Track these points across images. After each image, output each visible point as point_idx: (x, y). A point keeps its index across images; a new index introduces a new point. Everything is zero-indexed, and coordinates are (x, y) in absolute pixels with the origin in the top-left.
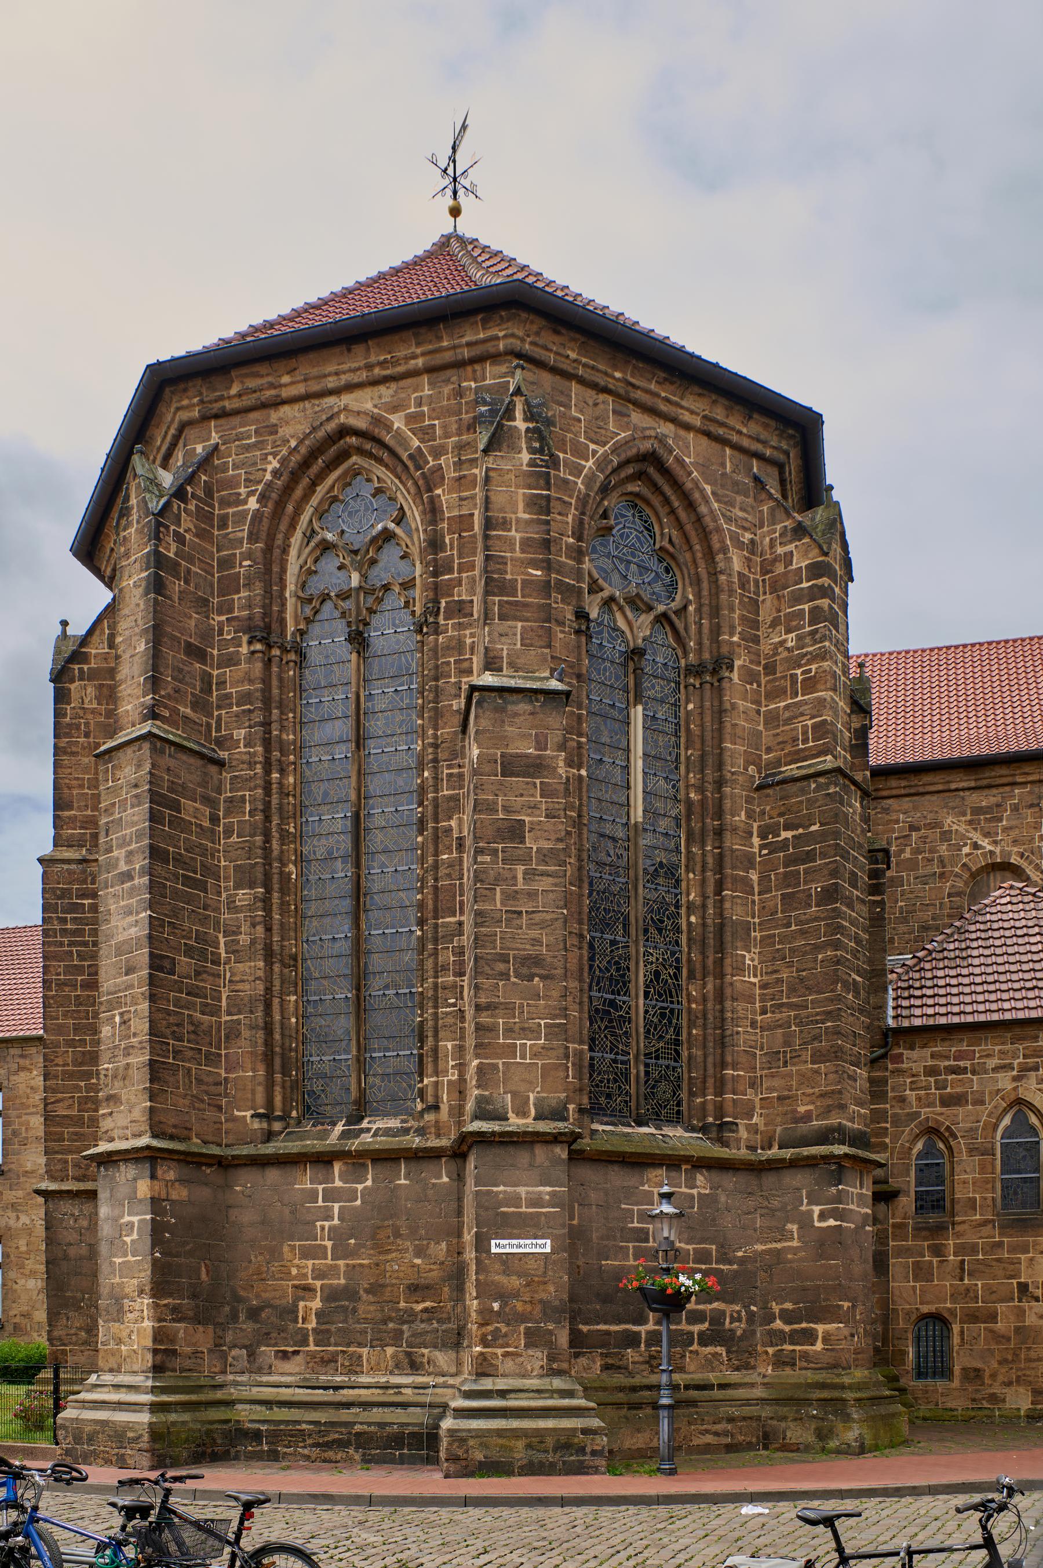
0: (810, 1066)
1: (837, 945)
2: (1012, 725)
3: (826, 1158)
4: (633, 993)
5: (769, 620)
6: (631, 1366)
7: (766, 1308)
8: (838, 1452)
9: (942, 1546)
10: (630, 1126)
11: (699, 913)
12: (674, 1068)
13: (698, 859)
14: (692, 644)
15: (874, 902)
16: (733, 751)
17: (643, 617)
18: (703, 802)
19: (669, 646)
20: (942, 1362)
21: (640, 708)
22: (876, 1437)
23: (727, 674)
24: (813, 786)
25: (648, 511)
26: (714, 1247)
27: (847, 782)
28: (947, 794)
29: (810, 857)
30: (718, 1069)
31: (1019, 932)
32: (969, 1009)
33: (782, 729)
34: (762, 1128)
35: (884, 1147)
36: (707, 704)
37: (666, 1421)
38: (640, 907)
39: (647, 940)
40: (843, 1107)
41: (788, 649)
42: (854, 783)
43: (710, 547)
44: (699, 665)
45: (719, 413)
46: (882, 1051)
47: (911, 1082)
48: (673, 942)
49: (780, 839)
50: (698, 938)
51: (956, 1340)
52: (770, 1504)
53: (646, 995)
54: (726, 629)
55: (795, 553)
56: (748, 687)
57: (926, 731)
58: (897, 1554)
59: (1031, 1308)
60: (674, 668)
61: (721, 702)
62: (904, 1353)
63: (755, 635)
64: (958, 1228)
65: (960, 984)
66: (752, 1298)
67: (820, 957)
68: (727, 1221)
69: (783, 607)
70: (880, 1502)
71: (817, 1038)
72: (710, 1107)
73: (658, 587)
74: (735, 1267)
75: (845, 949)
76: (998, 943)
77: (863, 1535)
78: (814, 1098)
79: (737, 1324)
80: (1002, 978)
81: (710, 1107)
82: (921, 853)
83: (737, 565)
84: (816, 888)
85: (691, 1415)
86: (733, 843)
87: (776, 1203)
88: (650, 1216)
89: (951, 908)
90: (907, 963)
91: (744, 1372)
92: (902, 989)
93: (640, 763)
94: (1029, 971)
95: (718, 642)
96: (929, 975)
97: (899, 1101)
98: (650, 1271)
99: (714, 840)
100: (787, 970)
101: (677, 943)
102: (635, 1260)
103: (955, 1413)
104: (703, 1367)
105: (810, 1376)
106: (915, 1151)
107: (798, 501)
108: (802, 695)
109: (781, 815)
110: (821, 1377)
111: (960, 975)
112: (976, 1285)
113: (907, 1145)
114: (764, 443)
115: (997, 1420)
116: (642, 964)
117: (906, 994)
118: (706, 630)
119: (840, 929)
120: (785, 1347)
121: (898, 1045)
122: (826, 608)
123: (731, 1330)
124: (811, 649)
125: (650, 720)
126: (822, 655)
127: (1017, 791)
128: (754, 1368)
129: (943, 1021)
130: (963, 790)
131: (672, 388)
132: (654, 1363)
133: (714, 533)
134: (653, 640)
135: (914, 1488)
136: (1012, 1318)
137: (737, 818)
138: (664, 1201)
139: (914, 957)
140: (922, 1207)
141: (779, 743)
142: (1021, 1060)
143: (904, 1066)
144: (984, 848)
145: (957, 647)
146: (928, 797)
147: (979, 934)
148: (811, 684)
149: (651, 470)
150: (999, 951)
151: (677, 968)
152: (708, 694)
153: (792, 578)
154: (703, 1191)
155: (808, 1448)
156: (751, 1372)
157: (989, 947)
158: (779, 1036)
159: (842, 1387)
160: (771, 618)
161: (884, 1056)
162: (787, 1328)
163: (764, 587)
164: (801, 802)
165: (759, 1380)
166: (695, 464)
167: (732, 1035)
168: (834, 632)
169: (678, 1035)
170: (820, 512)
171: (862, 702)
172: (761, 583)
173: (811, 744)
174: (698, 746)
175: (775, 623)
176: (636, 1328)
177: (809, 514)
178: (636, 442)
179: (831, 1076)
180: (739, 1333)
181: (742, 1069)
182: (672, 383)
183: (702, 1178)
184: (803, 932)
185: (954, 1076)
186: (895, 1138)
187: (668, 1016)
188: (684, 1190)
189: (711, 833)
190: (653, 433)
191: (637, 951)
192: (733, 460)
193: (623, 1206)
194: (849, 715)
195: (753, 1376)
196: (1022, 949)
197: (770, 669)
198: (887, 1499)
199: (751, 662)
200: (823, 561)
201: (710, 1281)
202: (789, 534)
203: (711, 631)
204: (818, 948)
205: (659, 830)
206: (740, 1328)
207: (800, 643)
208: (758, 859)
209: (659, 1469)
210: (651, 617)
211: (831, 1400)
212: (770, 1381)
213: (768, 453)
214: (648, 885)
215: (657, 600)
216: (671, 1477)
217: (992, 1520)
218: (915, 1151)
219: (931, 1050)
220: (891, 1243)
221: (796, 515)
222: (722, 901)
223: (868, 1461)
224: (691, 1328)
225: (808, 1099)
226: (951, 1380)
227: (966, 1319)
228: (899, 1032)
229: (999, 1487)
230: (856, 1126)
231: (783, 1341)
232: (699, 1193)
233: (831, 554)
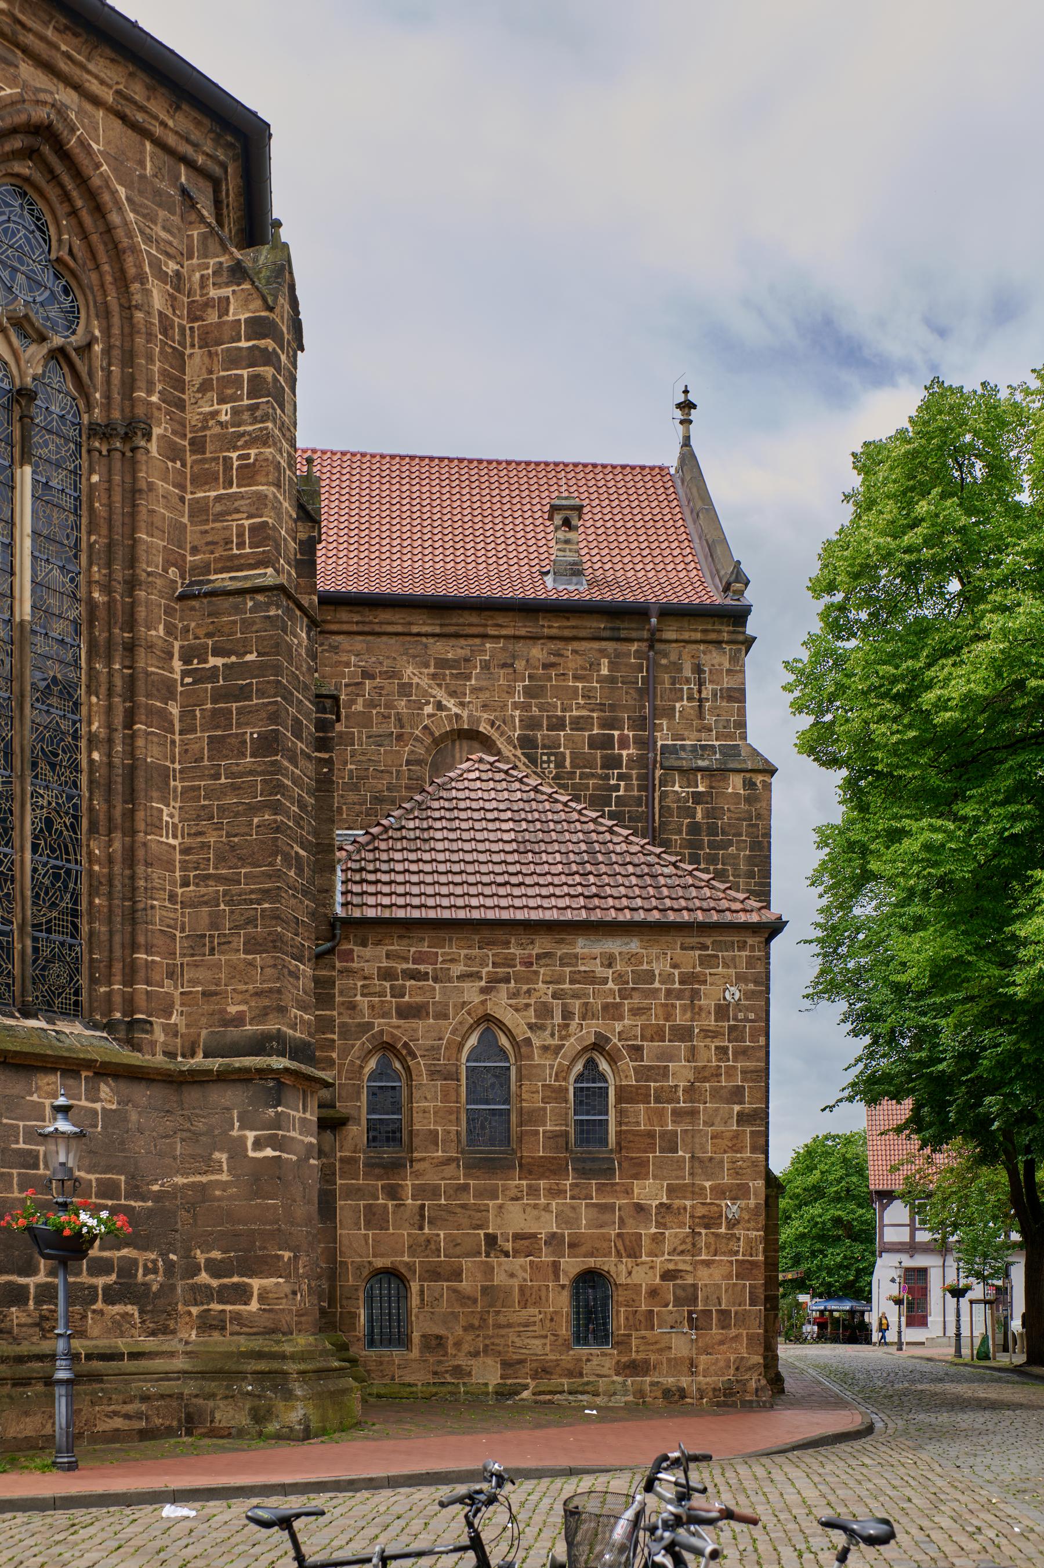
0: (243, 956)
1: (276, 808)
2: (484, 565)
3: (263, 1073)
4: (17, 844)
5: (197, 382)
6: (16, 1330)
7: (188, 1257)
8: (278, 1437)
9: (407, 1550)
10: (14, 1017)
11: (104, 748)
12: (71, 946)
13: (103, 678)
14: (98, 395)
15: (320, 759)
16: (150, 546)
17: (33, 348)
18: (110, 605)
19: (67, 394)
20: (399, 1326)
21: (28, 470)
22: (323, 1419)
23: (143, 443)
24: (250, 604)
25: (41, 205)
26: (123, 1178)
27: (292, 605)
28: (408, 638)
29: (243, 693)
30: (127, 952)
31: (490, 816)
32: (431, 902)
33: (211, 525)
34: (183, 1029)
35: (330, 1063)
36: (117, 478)
37: (63, 1400)
38: (27, 733)
39: (36, 777)
40: (282, 1010)
41: (220, 423)
42: (300, 607)
43: (123, 271)
44: (107, 426)
45: (138, 91)
46: (329, 945)
47: (362, 986)
48: (70, 783)
49: (207, 666)
50: (102, 781)
51: (415, 1301)
52: (198, 1505)
53: (35, 848)
54: (141, 384)
55: (232, 300)
56: (170, 464)
57: (384, 557)
58: (369, 1560)
59: (500, 1264)
60: (74, 424)
61: (135, 479)
62: (354, 1316)
63: (180, 398)
64: (417, 1166)
65: (421, 871)
66: (170, 1244)
67: (256, 820)
68: (140, 1146)
69: (215, 368)
70: (331, 1498)
71: (251, 922)
72: (117, 999)
73: (53, 311)
74: (150, 1204)
75: (287, 813)
76: (465, 825)
77: (313, 1540)
78: (247, 996)
79: (152, 1276)
80: (470, 868)
81: (117, 999)
82: (375, 707)
83: (158, 301)
84: (252, 734)
85: (94, 1393)
86: (148, 664)
87: (200, 1126)
88: (40, 1135)
89: (409, 779)
90: (359, 839)
91: (162, 1338)
92: (353, 870)
93: (28, 543)
94: (500, 863)
95: (131, 399)
96: (384, 856)
97: (348, 1008)
98: (42, 1206)
99: (123, 658)
100: (215, 833)
101: (75, 784)
102: (21, 1191)
103: (414, 1389)
104: (109, 1330)
105: (244, 1344)
106: (367, 1070)
107: (236, 234)
108: (238, 486)
109: (209, 635)
110: (257, 1344)
111: (421, 860)
112: (438, 1235)
113: (358, 1062)
114: (196, 146)
115: (462, 1397)
116: (28, 807)
117: (357, 878)
118: (116, 380)
119: (280, 788)
120: (212, 1306)
121: (347, 938)
122: (270, 379)
123: (144, 1284)
124: (250, 428)
125: (41, 488)
126: (263, 439)
127: (488, 645)
128: (173, 1332)
129: (401, 914)
130: (426, 635)
131: (76, 41)
132: (47, 1325)
133: (128, 253)
134: (47, 381)
135: (371, 1480)
136: (479, 1276)
137: (153, 633)
138: (59, 1116)
139: (367, 833)
140: (374, 1139)
141: (208, 544)
142: (490, 968)
143: (355, 965)
144: (449, 710)
145: (422, 458)
146: (384, 639)
147: (443, 812)
148: (249, 473)
149: (46, 149)
150: (466, 836)
151: (75, 817)
152: (117, 465)
153: (227, 333)
154: (109, 1106)
155: (241, 1433)
156: (170, 1337)
157: (455, 830)
158: (205, 916)
159: (283, 1357)
160: (200, 380)
161: (331, 951)
162: (215, 1283)
163: (192, 337)
164: (235, 622)
165: (181, 1347)
166: (104, 154)
167: (145, 909)
168: (279, 411)
169: (76, 903)
170: (264, 253)
171: (309, 508)
172: (188, 332)
173: (248, 550)
174: (104, 531)
175: (205, 387)
176: (22, 1280)
177: (251, 252)
178: (26, 106)
179: (269, 971)
180: (155, 1288)
181: (158, 954)
182: (76, 35)
183: (107, 1090)
184: (234, 787)
185: (413, 982)
186: (345, 1052)
187: (63, 878)
188: (84, 1103)
189: (120, 648)
190: (48, 98)
191: (23, 790)
192: (156, 162)
193: (5, 1121)
194: (295, 521)
195: (173, 1343)
196: (492, 836)
197: (198, 445)
198: (339, 1495)
199: (174, 433)
200: (267, 318)
201: (120, 1221)
202: (225, 274)
203: (123, 383)
204: (253, 809)
205: (52, 634)
206: (156, 1281)
207: (237, 418)
208: (180, 689)
209: (54, 1464)
210: (44, 349)
211: (270, 1372)
212: (195, 1349)
213: (200, 162)
214: (38, 705)
215: (52, 329)
216: (71, 1473)
217: (479, 1515)
218: (367, 1070)
219: (386, 948)
220: (339, 1182)
221: (234, 250)
222: (133, 737)
223: (314, 1448)
224: (94, 1281)
225: (240, 997)
226: (409, 1349)
227: (427, 1275)
228: (349, 923)
229: (485, 1475)
230: (298, 1035)
231: (210, 1299)
232: (103, 1109)
233: (277, 310)
